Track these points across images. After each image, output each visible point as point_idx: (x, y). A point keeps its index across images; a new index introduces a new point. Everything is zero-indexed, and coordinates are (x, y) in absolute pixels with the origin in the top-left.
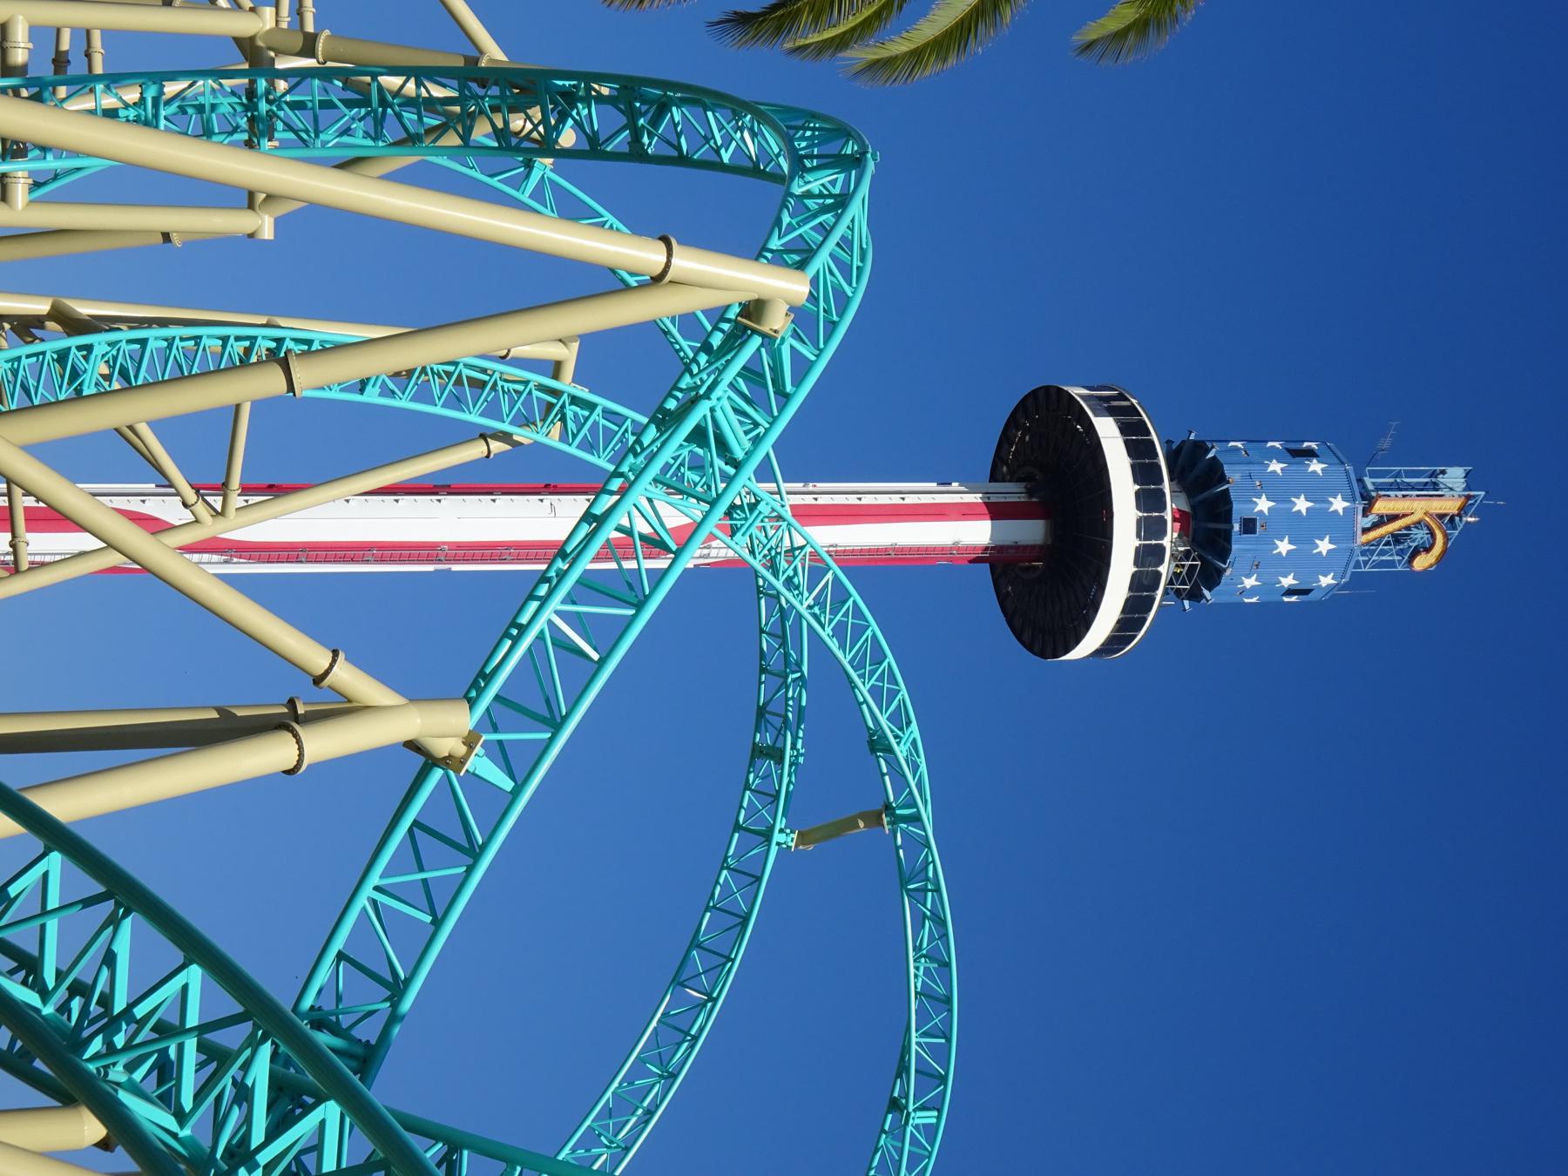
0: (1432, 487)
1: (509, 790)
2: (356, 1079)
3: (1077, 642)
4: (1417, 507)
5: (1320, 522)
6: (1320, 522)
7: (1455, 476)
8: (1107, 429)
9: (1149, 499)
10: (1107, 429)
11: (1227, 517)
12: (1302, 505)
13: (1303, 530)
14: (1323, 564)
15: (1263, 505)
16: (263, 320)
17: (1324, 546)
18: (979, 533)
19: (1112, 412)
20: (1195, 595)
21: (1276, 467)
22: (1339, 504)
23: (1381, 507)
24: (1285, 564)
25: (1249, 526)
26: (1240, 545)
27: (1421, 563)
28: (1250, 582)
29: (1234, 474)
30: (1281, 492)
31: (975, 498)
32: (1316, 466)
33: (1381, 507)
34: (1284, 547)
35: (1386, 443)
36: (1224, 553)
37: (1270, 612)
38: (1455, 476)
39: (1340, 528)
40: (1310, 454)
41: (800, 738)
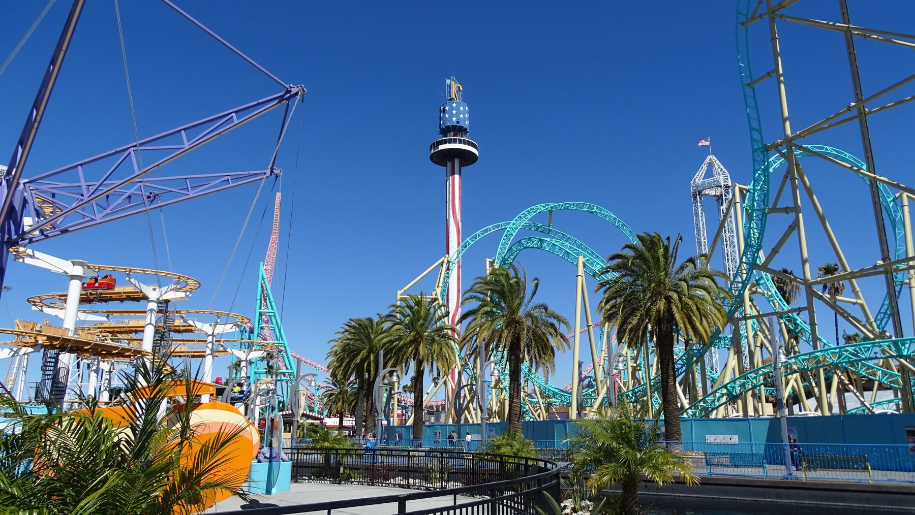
0: (450, 86)
1: (31, 218)
2: (390, 365)
3: (472, 152)
4: (454, 90)
5: (457, 109)
6: (457, 109)
7: (448, 81)
8: (441, 147)
9: (450, 141)
10: (441, 147)
11: (456, 126)
12: (454, 112)
13: (459, 112)
14: (464, 109)
15: (454, 119)
16: (22, 389)
17: (462, 108)
18: (457, 177)
19: (438, 146)
20: (467, 132)
21: (447, 116)
22: (454, 105)
23: (454, 97)
24: (464, 116)
25: (458, 122)
26: (461, 124)
27: (461, 89)
28: (467, 122)
29: (448, 124)
30: (452, 116)
31: (451, 178)
32: (447, 108)
33: (454, 97)
34: (461, 116)
35: (443, 94)
36: (462, 127)
37: (470, 119)
38: (448, 81)
39: (459, 105)
40: (444, 109)
41: (849, 384)
